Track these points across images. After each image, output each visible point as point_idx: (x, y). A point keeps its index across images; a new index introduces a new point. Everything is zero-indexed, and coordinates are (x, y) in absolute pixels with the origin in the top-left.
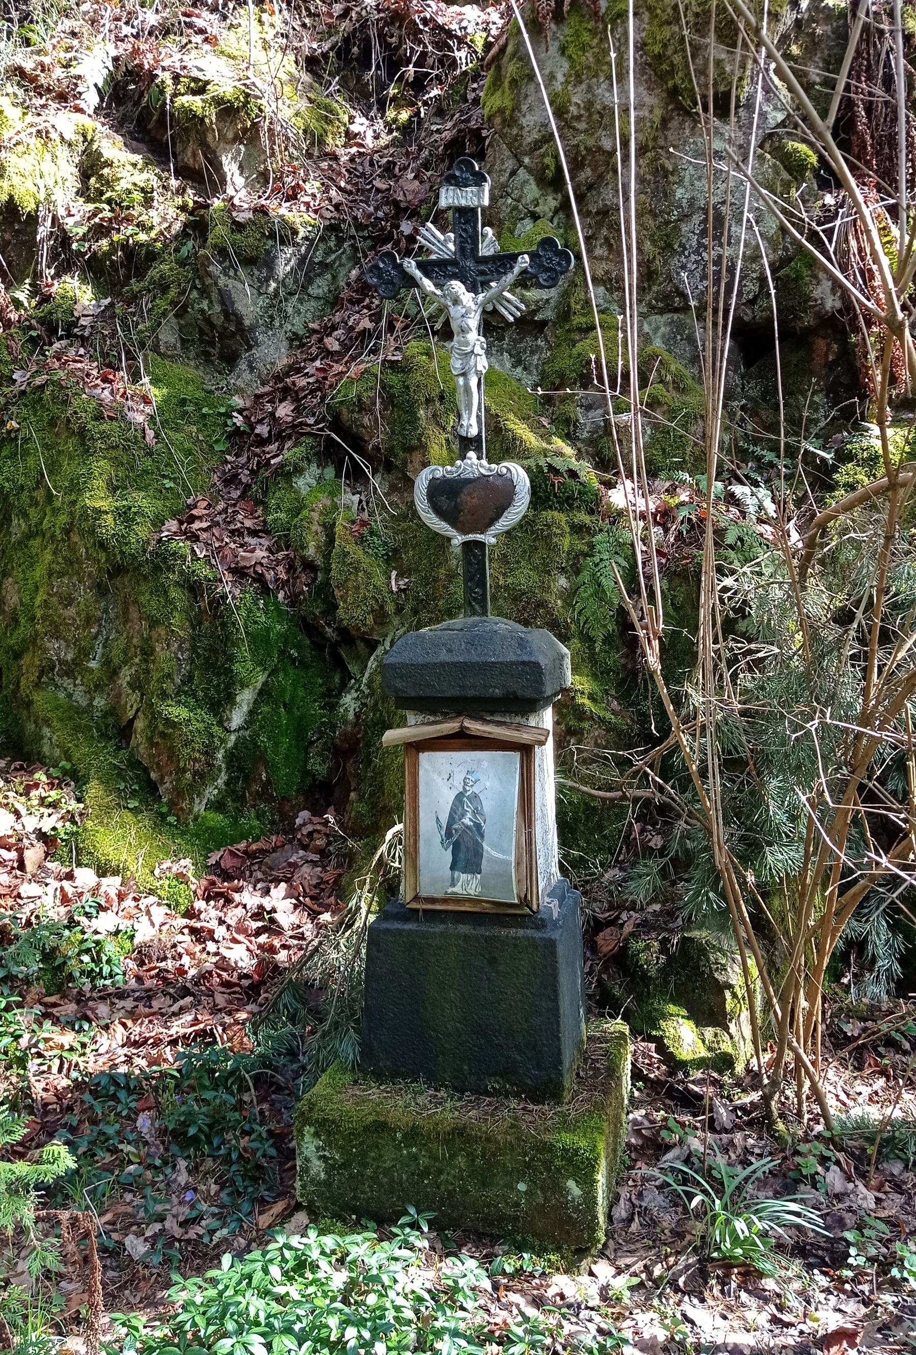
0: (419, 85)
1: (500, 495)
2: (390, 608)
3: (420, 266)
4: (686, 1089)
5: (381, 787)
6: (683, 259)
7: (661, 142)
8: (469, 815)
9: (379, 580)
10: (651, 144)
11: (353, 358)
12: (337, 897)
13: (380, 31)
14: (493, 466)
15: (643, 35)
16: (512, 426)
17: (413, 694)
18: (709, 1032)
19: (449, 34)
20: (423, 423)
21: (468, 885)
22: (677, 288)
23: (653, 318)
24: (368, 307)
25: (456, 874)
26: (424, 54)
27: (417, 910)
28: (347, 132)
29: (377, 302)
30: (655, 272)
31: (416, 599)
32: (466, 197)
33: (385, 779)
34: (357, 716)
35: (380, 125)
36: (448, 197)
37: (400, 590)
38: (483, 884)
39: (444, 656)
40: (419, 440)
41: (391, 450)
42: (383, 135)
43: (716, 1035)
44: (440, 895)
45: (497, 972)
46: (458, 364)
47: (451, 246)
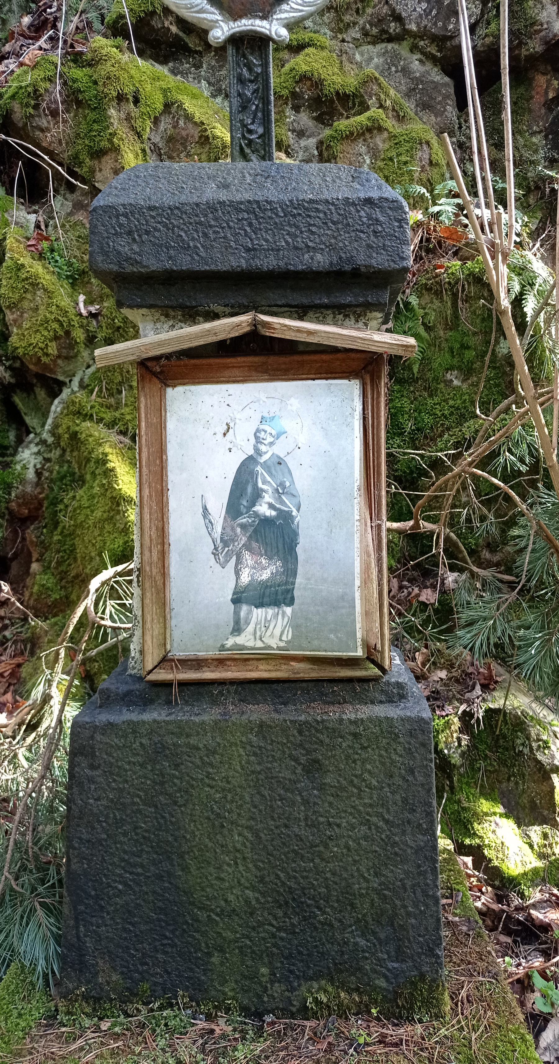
2: (79, 335)
4: (529, 918)
5: (73, 550)
8: (268, 498)
9: (65, 302)
12: (15, 692)
17: (153, 264)
18: (535, 832)
21: (269, 630)
22: (393, 10)
23: (365, 48)
25: (244, 608)
27: (167, 685)
33: (77, 541)
34: (38, 474)
38: (295, 624)
40: (110, 141)
43: (545, 836)
44: (213, 653)
45: (322, 788)
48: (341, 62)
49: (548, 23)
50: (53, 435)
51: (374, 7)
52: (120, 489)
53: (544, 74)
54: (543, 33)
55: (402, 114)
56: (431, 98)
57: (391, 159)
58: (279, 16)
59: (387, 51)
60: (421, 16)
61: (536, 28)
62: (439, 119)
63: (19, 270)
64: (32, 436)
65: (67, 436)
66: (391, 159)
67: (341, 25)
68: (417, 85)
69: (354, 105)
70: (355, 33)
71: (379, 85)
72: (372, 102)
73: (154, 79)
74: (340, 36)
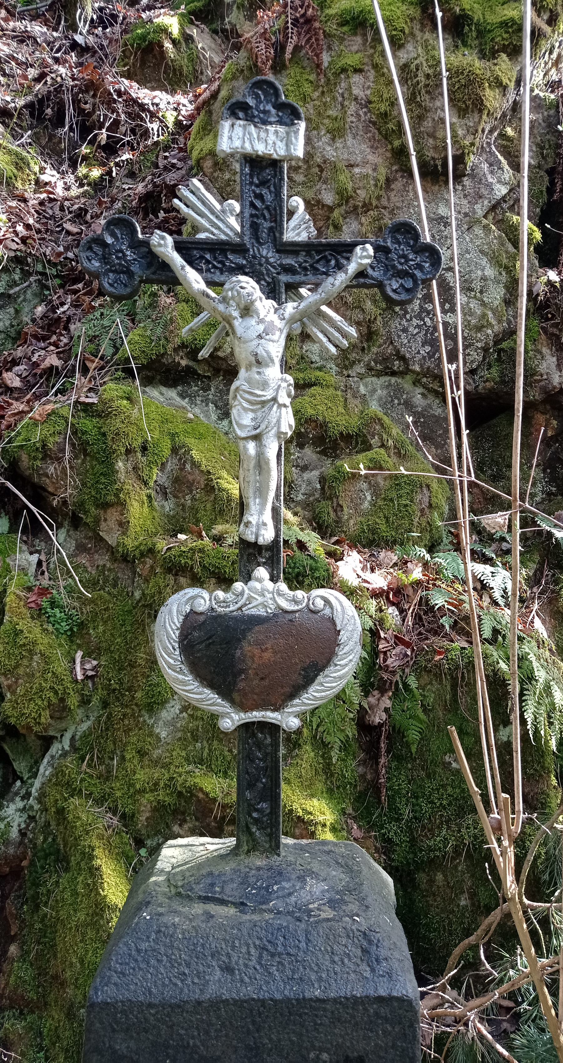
0: (111, 149)
1: (312, 646)
2: (73, 701)
3: (179, 247)
6: (404, 322)
7: (384, 202)
9: (61, 666)
10: (374, 203)
11: (37, 397)
13: (75, 96)
14: (300, 594)
15: (368, 92)
16: (225, 485)
19: (142, 107)
20: (122, 476)
22: (398, 352)
23: (369, 380)
24: (56, 345)
26: (116, 124)
28: (37, 182)
29: (65, 340)
30: (376, 333)
31: (107, 688)
32: (269, 141)
34: (22, 834)
35: (70, 179)
36: (234, 138)
37: (87, 677)
39: (217, 985)
40: (117, 496)
41: (81, 505)
42: (73, 187)
46: (247, 419)
47: (233, 221)
48: (346, 400)
49: (547, 374)
50: (40, 802)
51: (380, 346)
52: (105, 896)
53: (543, 413)
54: (543, 383)
55: (403, 452)
56: (432, 431)
57: (392, 500)
58: (290, 710)
59: (390, 385)
60: (424, 358)
61: (536, 378)
62: (439, 451)
63: (17, 635)
64: (18, 783)
65: (53, 809)
66: (392, 500)
67: (347, 363)
68: (419, 418)
69: (357, 443)
70: (359, 369)
71: (382, 425)
72: (375, 441)
73: (163, 422)
74: (345, 372)
